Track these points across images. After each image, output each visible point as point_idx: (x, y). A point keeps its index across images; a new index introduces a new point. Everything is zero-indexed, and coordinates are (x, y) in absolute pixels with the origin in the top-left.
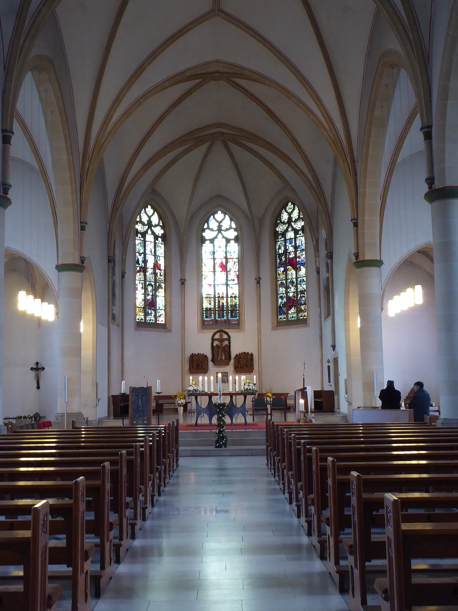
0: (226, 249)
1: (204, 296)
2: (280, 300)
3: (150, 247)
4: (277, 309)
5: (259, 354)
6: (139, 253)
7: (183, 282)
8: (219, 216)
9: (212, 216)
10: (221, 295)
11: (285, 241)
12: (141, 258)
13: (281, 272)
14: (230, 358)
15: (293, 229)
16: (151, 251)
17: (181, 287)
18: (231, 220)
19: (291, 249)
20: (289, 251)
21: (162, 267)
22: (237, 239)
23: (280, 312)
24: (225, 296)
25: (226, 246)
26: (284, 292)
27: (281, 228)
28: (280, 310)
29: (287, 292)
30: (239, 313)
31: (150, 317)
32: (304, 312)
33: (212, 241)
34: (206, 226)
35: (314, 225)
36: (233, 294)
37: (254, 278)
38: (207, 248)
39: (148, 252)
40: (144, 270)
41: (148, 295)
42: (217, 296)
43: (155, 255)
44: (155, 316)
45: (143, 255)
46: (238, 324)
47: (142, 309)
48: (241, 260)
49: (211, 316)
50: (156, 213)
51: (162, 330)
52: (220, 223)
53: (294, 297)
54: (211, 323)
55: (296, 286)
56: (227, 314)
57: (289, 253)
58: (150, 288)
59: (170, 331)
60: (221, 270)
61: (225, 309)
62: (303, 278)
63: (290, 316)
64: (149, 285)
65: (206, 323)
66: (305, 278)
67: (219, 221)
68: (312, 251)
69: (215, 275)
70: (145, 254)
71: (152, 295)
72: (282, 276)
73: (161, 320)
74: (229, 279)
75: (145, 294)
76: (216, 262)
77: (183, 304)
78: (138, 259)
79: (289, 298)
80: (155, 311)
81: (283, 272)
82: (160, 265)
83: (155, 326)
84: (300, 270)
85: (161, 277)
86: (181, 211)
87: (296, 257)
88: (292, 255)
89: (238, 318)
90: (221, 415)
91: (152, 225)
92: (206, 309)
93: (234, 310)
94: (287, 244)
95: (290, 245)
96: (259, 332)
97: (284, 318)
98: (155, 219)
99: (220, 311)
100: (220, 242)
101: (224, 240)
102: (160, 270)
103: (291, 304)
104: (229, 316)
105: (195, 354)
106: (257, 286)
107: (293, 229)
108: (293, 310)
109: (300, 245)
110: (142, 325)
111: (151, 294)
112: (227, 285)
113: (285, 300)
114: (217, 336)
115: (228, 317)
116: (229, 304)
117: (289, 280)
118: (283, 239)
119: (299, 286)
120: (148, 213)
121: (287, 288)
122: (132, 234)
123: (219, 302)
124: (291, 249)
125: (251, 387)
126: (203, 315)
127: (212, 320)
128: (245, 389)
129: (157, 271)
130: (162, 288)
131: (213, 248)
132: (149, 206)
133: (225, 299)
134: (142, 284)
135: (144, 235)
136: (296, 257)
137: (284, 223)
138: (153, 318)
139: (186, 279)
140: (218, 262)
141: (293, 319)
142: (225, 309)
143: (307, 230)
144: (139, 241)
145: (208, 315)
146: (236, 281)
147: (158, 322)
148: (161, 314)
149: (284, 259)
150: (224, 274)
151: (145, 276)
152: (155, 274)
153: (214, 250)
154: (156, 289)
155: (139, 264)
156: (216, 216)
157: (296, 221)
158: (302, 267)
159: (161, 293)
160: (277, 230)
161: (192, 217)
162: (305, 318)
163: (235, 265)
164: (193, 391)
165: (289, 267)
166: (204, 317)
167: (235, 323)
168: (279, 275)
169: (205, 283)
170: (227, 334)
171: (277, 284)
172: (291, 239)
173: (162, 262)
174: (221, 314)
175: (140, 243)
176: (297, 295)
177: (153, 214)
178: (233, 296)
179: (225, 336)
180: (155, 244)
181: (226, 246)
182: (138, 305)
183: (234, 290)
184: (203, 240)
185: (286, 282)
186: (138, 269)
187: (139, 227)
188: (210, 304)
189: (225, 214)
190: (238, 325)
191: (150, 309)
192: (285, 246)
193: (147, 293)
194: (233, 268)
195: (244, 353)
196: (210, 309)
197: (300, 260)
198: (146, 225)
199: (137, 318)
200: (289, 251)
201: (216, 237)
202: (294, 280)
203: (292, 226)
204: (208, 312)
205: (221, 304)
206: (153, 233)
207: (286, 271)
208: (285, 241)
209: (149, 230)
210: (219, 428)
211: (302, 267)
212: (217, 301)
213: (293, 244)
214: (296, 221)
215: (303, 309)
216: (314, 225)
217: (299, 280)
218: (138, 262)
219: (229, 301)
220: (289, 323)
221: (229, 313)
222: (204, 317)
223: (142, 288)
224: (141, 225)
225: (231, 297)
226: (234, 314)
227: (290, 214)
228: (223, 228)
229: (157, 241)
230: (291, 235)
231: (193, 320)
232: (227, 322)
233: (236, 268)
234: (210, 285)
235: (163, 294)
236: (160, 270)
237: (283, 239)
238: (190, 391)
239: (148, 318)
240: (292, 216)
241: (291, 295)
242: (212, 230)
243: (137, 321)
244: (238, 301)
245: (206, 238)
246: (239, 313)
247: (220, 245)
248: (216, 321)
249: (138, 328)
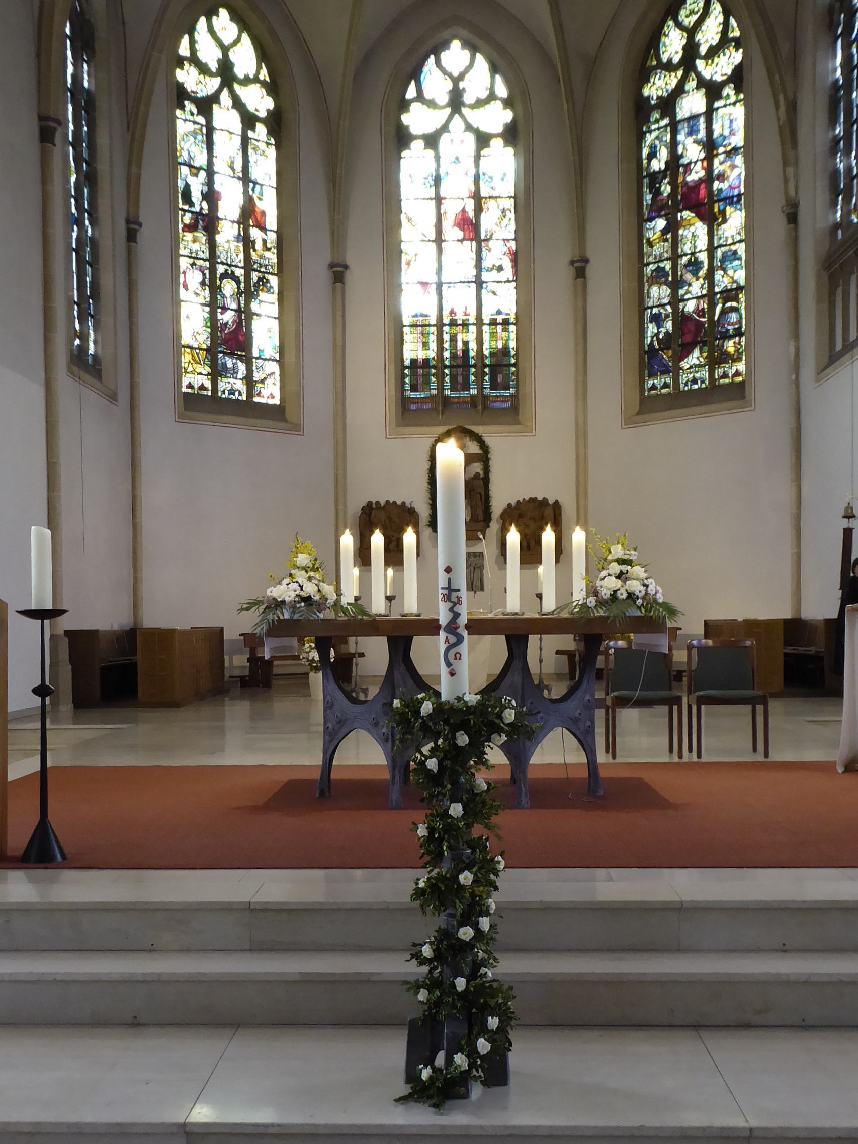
0: (477, 165)
1: (406, 320)
2: (651, 329)
3: (227, 147)
4: (641, 358)
5: (582, 503)
6: (190, 166)
7: (338, 273)
8: (455, 55)
9: (432, 58)
10: (460, 317)
11: (674, 127)
12: (197, 186)
13: (658, 234)
15: (702, 83)
16: (227, 159)
17: (334, 289)
18: (494, 69)
19: (692, 151)
20: (685, 161)
21: (271, 222)
22: (511, 134)
23: (651, 367)
24: (472, 319)
25: (478, 157)
26: (666, 301)
27: (658, 86)
28: (651, 360)
29: (675, 300)
30: (517, 374)
31: (232, 381)
32: (734, 361)
33: (432, 141)
34: (411, 92)
35: (785, 48)
36: (499, 312)
37: (567, 259)
38: (414, 163)
39: (220, 165)
40: (208, 224)
41: (225, 309)
42: (446, 320)
43: (246, 178)
44: (249, 380)
45: (203, 174)
46: (515, 409)
47: (203, 354)
48: (525, 204)
49: (428, 383)
50: (245, 37)
51: (270, 423)
52: (456, 80)
53: (699, 312)
55: (710, 277)
56: (480, 376)
57: (687, 167)
58: (229, 287)
59: (297, 428)
60: (461, 234)
61: (472, 362)
62: (733, 248)
63: (683, 378)
64: (225, 275)
65: (413, 407)
66: (741, 249)
67: (456, 74)
68: (772, 147)
69: (440, 251)
70: (210, 173)
71: (238, 311)
72: (661, 249)
73: (270, 393)
74: (486, 264)
75: (214, 305)
76: (443, 208)
77: (339, 343)
78: (187, 186)
79: (681, 319)
80: (248, 361)
81: (664, 232)
82: (263, 214)
83: (248, 410)
84: (725, 221)
85: (267, 254)
86: (332, 37)
87: (710, 177)
88: (697, 174)
89: (512, 391)
90: (456, 810)
91: (234, 78)
92: (414, 362)
93: (500, 363)
94: (681, 137)
95: (690, 140)
96: (581, 434)
97: (666, 385)
98: (245, 59)
99: (458, 367)
100: (458, 143)
101: (471, 138)
102: (263, 229)
103: (688, 338)
104: (487, 385)
105: (378, 503)
106: (575, 286)
107: (702, 83)
108: (695, 358)
109: (726, 133)
110: (195, 404)
111: (234, 306)
112: (479, 283)
113: (669, 325)
115: (481, 388)
116: (486, 346)
117: (685, 260)
118: (666, 121)
119: (718, 275)
120: (220, 34)
121: (677, 284)
122: (160, 95)
123: (453, 339)
124: (692, 151)
125: (635, 587)
126: (404, 383)
127: (432, 396)
128: (605, 594)
129: (255, 233)
130: (269, 290)
131: (434, 165)
132: (223, 12)
133: (473, 329)
134: (201, 269)
135: (205, 105)
136: (710, 177)
137: (669, 67)
138: (240, 385)
139: (348, 263)
140: (451, 210)
141: (696, 387)
143: (758, 76)
144: (190, 127)
145: (420, 381)
146: (508, 273)
147: (256, 399)
148: (268, 372)
149: (666, 189)
150: (469, 246)
151: (212, 245)
152: (248, 243)
153: (437, 170)
154: (248, 292)
155: (191, 204)
156: (444, 56)
157: (713, 52)
158: (729, 210)
159: (266, 307)
160: (646, 92)
161: (367, 61)
162: (740, 379)
163: (506, 221)
164: (293, 606)
165: (686, 214)
167: (504, 405)
168: (650, 244)
169: (409, 277)
170: (479, 439)
171: (641, 274)
172: (694, 118)
173: (268, 204)
174: (460, 379)
175: (194, 134)
176: (712, 306)
177: (237, 41)
178: (500, 319)
180: (245, 142)
181: (478, 157)
182: (186, 339)
183: (503, 299)
184: (403, 138)
185: (674, 267)
186: (187, 219)
187: (187, 77)
188: (425, 345)
189: (474, 49)
190: (513, 413)
191: (232, 355)
192: (674, 144)
193: (220, 303)
194: (496, 228)
195: (533, 500)
196: (426, 361)
197: (724, 186)
198: (212, 75)
200: (685, 161)
201: (445, 128)
202: (703, 257)
203: (699, 75)
204: (420, 371)
205: (460, 345)
206: (238, 104)
207: (673, 227)
208: (674, 127)
209: (225, 92)
210: (441, 920)
211: (729, 210)
212: (446, 337)
213: (702, 134)
214: (713, 52)
215: (731, 350)
216: (785, 48)
217: (719, 253)
218: (187, 196)
219: (486, 337)
220: (681, 400)
221: (485, 374)
222: (407, 387)
223: (203, 283)
224: (193, 71)
225: (493, 323)
226: (500, 379)
227: (691, 32)
228: (468, 98)
229: (250, 134)
230: (693, 103)
231: (371, 396)
232: (480, 405)
233: (509, 230)
234: (424, 284)
235: (274, 310)
236: (263, 229)
237: (666, 121)
238: (279, 604)
239: (224, 384)
240: (699, 37)
241: (690, 306)
242: (431, 104)
244: (513, 336)
245: (414, 131)
246: (517, 374)
247: (459, 144)
248: (446, 400)
249: (189, 413)
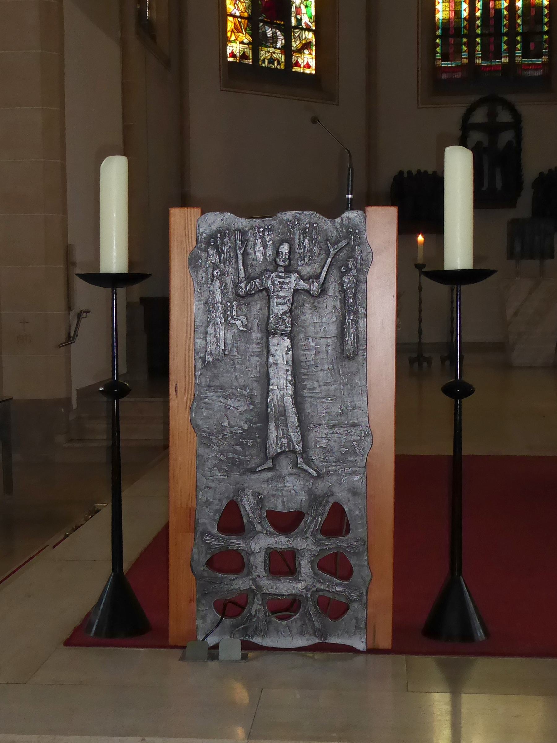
14: (519, 186)
44: (287, 50)
49: (460, 51)
54: (458, 75)
61: (505, 30)
65: (444, 76)
80: (288, 31)
83: (286, 78)
89: (544, 58)
99: (490, 35)
104: (519, 53)
105: (409, 172)
110: (245, 74)
114: (480, 116)
115: (512, 56)
142: (505, 30)
166: (438, 56)
179: (504, 117)
191: (271, 24)
199: (229, 51)
204: (452, 40)
222: (438, 56)
226: (532, 47)
243: (230, 59)
246: (549, 41)
